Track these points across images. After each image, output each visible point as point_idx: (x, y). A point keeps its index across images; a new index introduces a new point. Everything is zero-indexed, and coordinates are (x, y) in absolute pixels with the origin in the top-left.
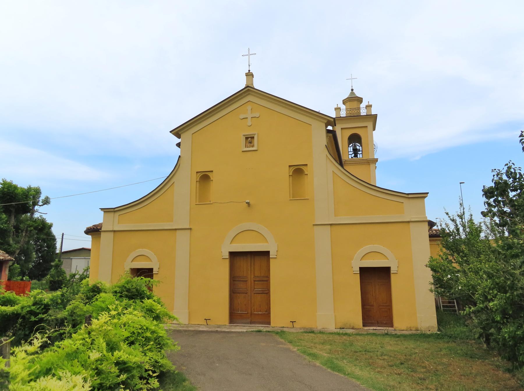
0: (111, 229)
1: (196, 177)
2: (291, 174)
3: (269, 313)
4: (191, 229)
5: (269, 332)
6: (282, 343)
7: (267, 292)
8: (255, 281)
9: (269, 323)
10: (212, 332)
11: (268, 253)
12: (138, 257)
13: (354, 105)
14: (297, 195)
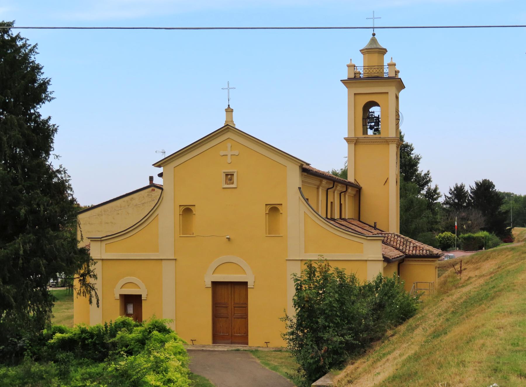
0: (100, 258)
1: (179, 211)
2: (267, 212)
3: (247, 335)
4: (176, 260)
5: (245, 350)
6: (253, 358)
7: (245, 317)
8: (235, 307)
9: (247, 344)
10: (199, 350)
11: (246, 283)
12: (128, 284)
13: (374, 59)
14: (272, 229)
